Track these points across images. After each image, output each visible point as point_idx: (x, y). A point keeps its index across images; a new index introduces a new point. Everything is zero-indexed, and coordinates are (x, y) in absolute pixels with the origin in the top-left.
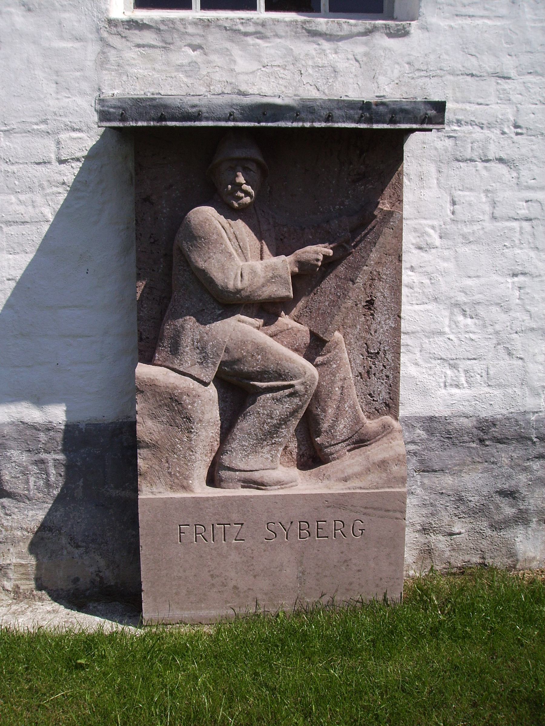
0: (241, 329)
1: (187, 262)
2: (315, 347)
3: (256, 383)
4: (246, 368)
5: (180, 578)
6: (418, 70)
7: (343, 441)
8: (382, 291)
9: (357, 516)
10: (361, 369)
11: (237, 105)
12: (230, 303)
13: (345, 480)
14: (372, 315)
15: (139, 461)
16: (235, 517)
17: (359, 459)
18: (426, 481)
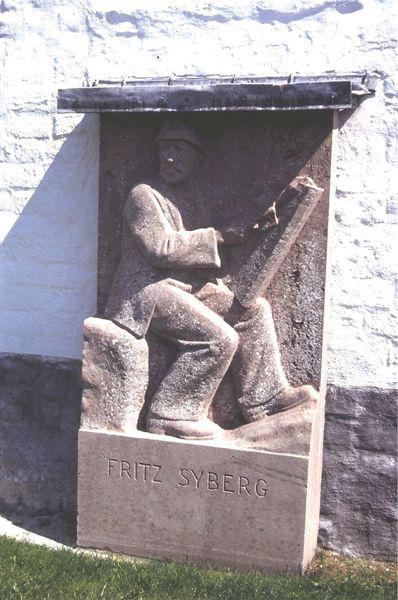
0: (173, 291)
1: (130, 231)
2: (237, 313)
3: (182, 342)
4: (172, 326)
5: (108, 508)
6: (370, 42)
7: (263, 404)
8: (307, 264)
9: (261, 476)
10: (286, 337)
11: (164, 92)
12: (165, 267)
13: (254, 440)
14: (298, 286)
15: (83, 398)
16: (154, 459)
17: (272, 422)
18: (366, 459)
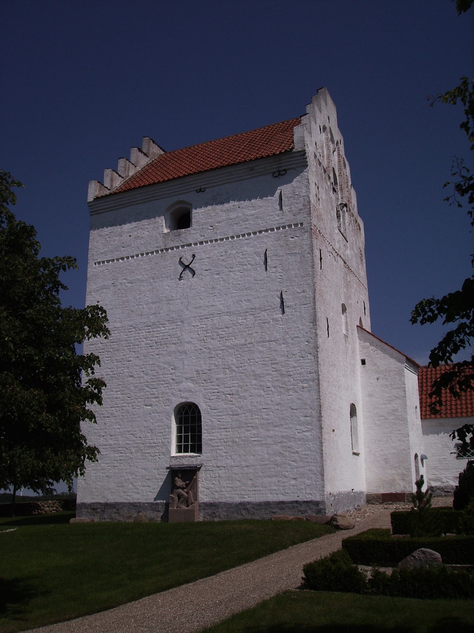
0: (180, 490)
2: (187, 493)
